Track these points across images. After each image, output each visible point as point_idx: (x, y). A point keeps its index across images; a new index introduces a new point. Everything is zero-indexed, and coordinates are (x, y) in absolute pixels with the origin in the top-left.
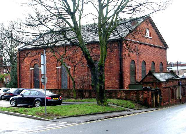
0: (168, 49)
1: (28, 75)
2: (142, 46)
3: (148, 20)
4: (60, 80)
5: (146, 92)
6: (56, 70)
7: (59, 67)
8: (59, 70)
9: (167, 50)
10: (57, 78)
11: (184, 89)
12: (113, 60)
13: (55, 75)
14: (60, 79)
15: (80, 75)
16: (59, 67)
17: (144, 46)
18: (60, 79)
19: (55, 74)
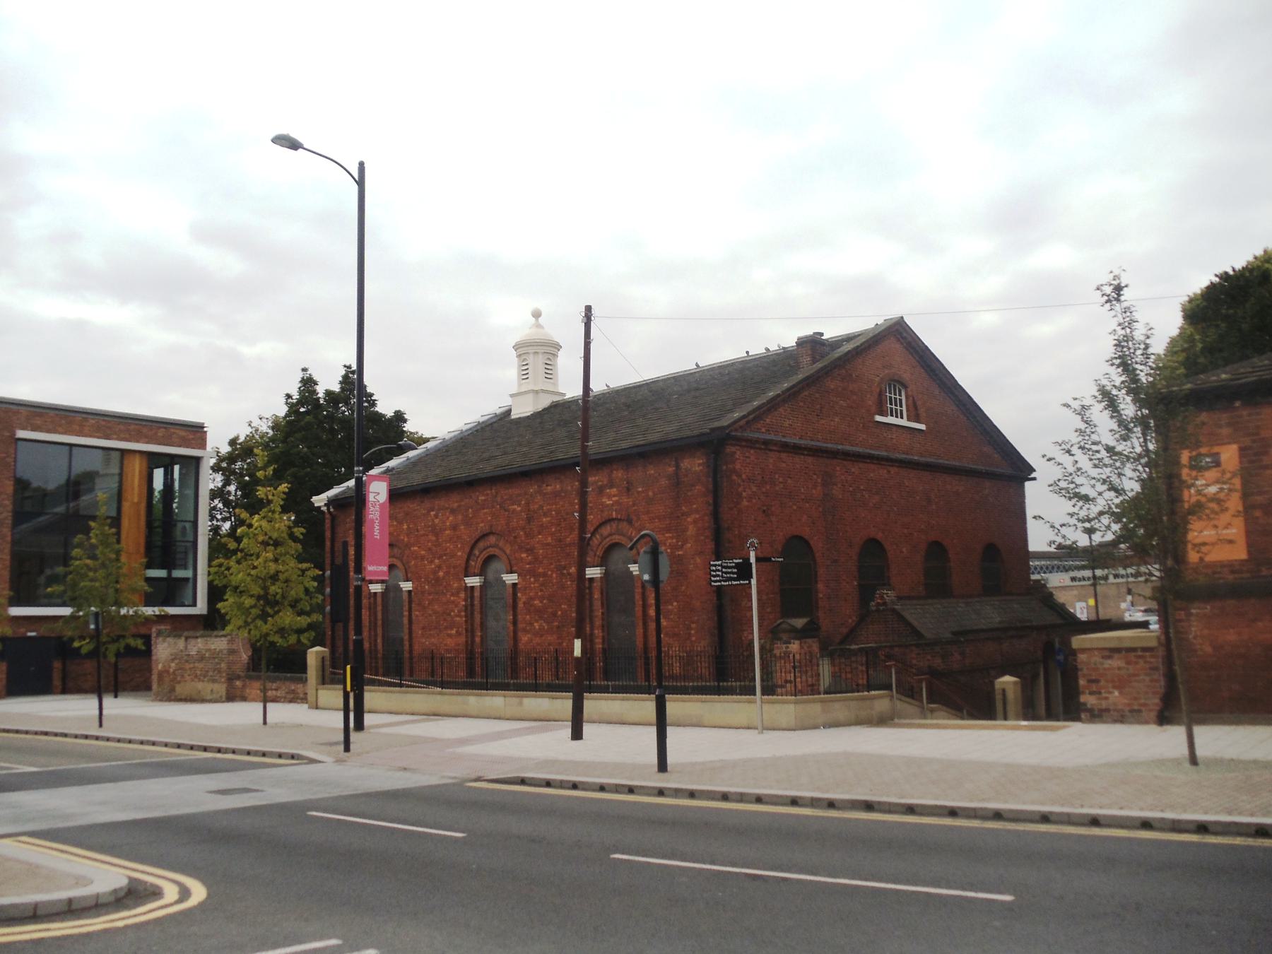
0: (1034, 479)
1: (598, 670)
2: (861, 465)
3: (517, 347)
4: (478, 640)
5: (788, 685)
6: (462, 595)
7: (473, 581)
8: (477, 594)
9: (1027, 484)
10: (467, 630)
11: (580, 612)
12: (685, 542)
13: (458, 619)
14: (479, 634)
15: (554, 614)
16: (473, 581)
17: (873, 466)
18: (479, 634)
19: (459, 611)
